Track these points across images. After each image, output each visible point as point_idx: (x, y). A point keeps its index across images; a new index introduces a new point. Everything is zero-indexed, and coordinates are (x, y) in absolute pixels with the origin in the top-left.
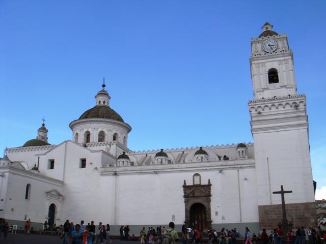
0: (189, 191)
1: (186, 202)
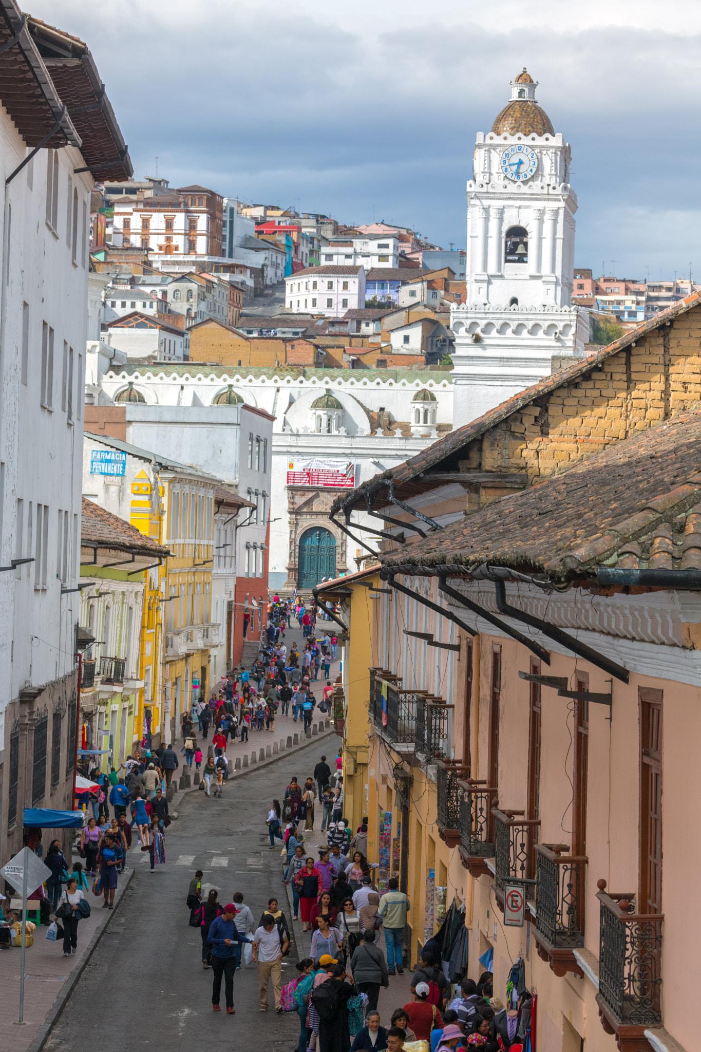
0: (300, 500)
1: (295, 524)
